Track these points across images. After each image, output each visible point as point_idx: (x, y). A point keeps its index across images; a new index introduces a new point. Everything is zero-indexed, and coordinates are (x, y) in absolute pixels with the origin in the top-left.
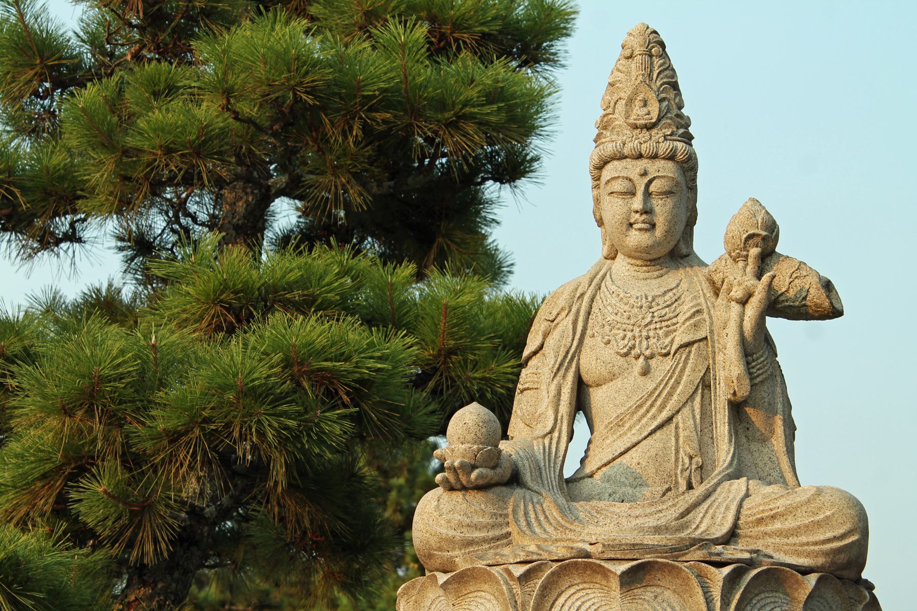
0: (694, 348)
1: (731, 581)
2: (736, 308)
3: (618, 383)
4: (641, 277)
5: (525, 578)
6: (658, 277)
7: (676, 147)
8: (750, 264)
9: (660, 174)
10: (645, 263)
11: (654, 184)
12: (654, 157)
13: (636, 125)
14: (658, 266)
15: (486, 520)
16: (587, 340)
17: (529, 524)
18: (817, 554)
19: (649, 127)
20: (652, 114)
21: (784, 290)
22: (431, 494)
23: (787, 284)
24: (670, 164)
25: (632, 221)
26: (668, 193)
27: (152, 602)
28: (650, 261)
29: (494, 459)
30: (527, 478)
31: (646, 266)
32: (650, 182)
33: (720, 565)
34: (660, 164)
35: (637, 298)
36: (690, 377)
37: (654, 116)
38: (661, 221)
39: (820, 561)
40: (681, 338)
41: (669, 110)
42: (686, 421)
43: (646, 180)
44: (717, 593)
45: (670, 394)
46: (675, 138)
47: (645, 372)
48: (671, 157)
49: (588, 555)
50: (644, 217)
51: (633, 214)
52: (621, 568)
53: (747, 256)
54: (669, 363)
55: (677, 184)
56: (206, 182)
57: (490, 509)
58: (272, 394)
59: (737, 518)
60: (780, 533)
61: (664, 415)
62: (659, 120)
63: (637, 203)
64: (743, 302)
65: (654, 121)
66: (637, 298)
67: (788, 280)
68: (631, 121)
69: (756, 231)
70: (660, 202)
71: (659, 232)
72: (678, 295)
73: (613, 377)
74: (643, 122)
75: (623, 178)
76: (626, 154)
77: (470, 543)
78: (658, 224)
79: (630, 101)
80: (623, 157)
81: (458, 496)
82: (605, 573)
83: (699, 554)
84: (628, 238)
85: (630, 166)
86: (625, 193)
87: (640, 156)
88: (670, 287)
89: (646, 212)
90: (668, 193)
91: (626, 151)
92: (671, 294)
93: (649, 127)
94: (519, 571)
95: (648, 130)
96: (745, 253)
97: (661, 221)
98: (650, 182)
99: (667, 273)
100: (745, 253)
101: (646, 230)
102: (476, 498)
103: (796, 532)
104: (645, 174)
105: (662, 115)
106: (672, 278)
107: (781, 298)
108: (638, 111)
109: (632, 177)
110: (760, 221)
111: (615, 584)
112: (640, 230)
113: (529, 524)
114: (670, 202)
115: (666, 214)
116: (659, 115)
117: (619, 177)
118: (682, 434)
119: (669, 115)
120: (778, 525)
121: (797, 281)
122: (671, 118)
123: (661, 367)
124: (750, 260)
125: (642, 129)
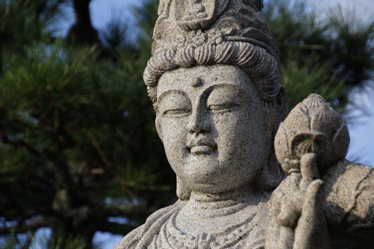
2: (284, 232)
4: (208, 214)
6: (229, 213)
7: (237, 49)
8: (303, 174)
9: (218, 83)
10: (213, 197)
11: (211, 96)
12: (210, 62)
13: (187, 25)
14: (230, 202)
20: (207, 11)
21: (350, 206)
23: (353, 198)
24: (230, 70)
25: (188, 144)
26: (228, 106)
28: (220, 194)
31: (215, 200)
32: (207, 93)
35: (193, 238)
37: (210, 11)
43: (201, 91)
46: (237, 38)
50: (201, 136)
51: (189, 135)
53: (298, 166)
55: (241, 94)
56: (202, 245)
62: (216, 17)
63: (191, 121)
65: (209, 18)
66: (193, 238)
67: (354, 193)
68: (183, 21)
69: (306, 131)
70: (220, 117)
71: (222, 155)
72: (245, 231)
74: (196, 21)
75: (175, 91)
76: (177, 63)
78: (219, 146)
84: (186, 167)
85: (183, 77)
86: (178, 111)
87: (193, 64)
88: (238, 223)
89: (202, 132)
91: (177, 60)
92: (236, 231)
93: (204, 27)
95: (203, 31)
96: (295, 161)
98: (207, 93)
99: (242, 208)
100: (295, 161)
101: (205, 153)
104: (199, 83)
105: (220, 11)
107: (350, 219)
109: (184, 89)
110: (313, 118)
112: (198, 153)
114: (232, 117)
115: (228, 132)
116: (215, 11)
117: (170, 92)
119: (231, 11)
121: (365, 194)
122: (233, 15)
124: (303, 169)
125: (196, 30)
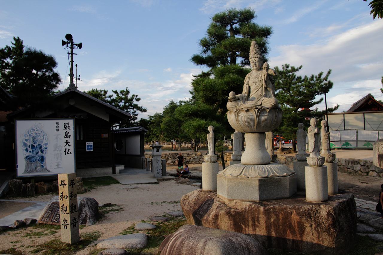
0: (261, 81)
1: (258, 111)
2: (264, 76)
3: (252, 86)
5: (236, 112)
12: (256, 58)
15: (234, 105)
16: (250, 81)
17: (239, 105)
18: (269, 106)
19: (255, 54)
22: (228, 102)
26: (258, 62)
27: (77, 177)
29: (235, 98)
30: (240, 99)
33: (257, 109)
34: (256, 58)
36: (261, 85)
38: (257, 66)
39: (271, 107)
40: (260, 80)
41: (257, 51)
42: (260, 90)
44: (257, 112)
45: (258, 87)
47: (256, 84)
48: (258, 57)
49: (242, 109)
52: (246, 110)
54: (258, 83)
57: (234, 103)
58: (87, 206)
59: (262, 102)
60: (266, 104)
61: (257, 90)
63: (254, 63)
64: (265, 75)
71: (257, 67)
73: (252, 85)
77: (232, 107)
79: (252, 51)
80: (252, 58)
81: (231, 102)
82: (244, 111)
83: (254, 108)
90: (258, 62)
93: (255, 54)
94: (235, 111)
97: (257, 66)
102: (233, 102)
103: (268, 104)
104: (255, 60)
106: (260, 72)
108: (253, 52)
111: (245, 112)
113: (239, 105)
118: (260, 92)
120: (266, 103)
123: (257, 83)
